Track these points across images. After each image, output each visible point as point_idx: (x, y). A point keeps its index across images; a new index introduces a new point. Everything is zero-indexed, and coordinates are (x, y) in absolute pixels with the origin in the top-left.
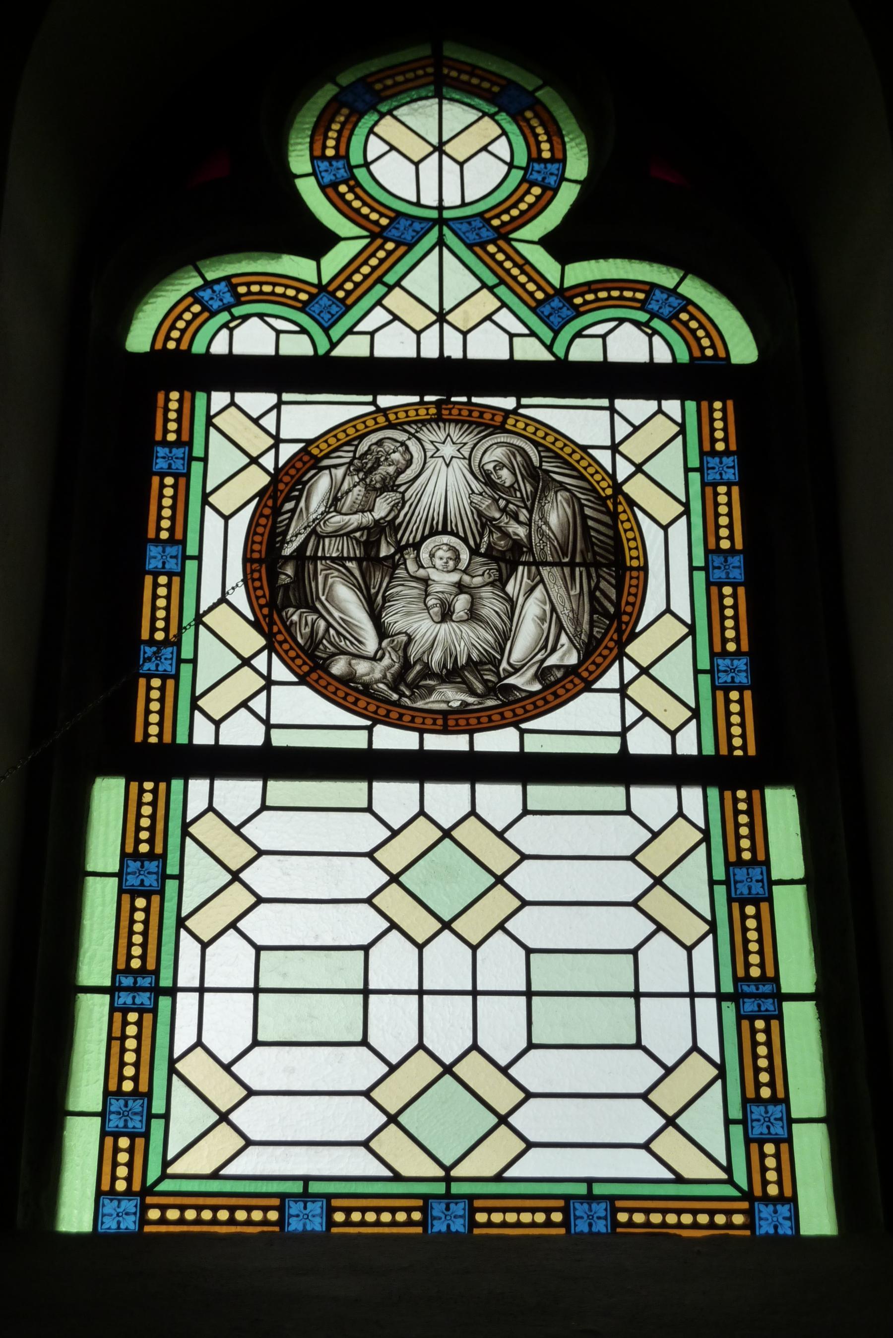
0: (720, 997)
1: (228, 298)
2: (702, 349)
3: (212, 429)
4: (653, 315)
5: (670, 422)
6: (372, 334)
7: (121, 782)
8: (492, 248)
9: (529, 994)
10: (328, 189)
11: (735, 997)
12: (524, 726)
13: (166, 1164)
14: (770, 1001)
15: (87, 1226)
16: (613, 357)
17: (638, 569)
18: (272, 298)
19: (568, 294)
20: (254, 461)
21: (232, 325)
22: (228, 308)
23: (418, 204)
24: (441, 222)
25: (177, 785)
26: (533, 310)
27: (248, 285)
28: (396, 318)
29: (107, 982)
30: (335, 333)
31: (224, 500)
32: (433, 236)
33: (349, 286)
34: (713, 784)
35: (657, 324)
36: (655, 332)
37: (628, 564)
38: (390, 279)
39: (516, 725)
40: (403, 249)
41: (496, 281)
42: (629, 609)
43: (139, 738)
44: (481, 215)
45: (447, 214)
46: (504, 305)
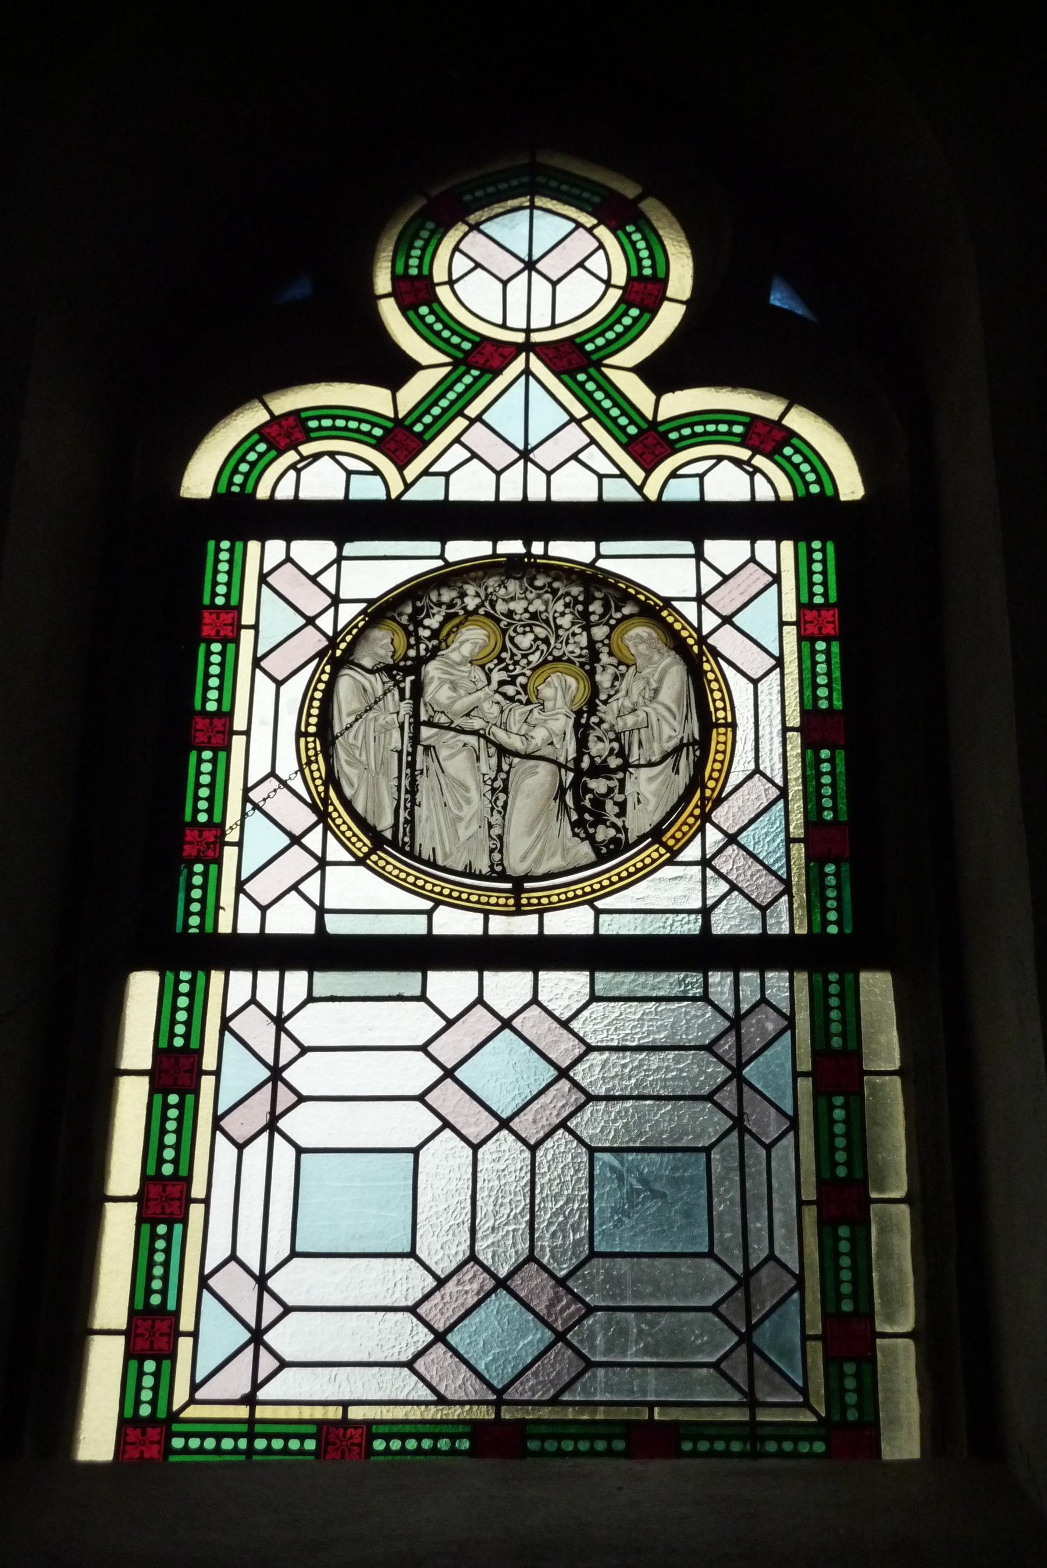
2: (807, 484)
6: (447, 475)
13: (195, 1387)
16: (710, 496)
19: (662, 429)
21: (299, 466)
24: (528, 347)
25: (217, 977)
28: (474, 455)
30: (412, 471)
34: (801, 968)
35: (759, 461)
36: (757, 470)
38: (472, 411)
41: (585, 413)
43: (179, 928)
46: (593, 441)
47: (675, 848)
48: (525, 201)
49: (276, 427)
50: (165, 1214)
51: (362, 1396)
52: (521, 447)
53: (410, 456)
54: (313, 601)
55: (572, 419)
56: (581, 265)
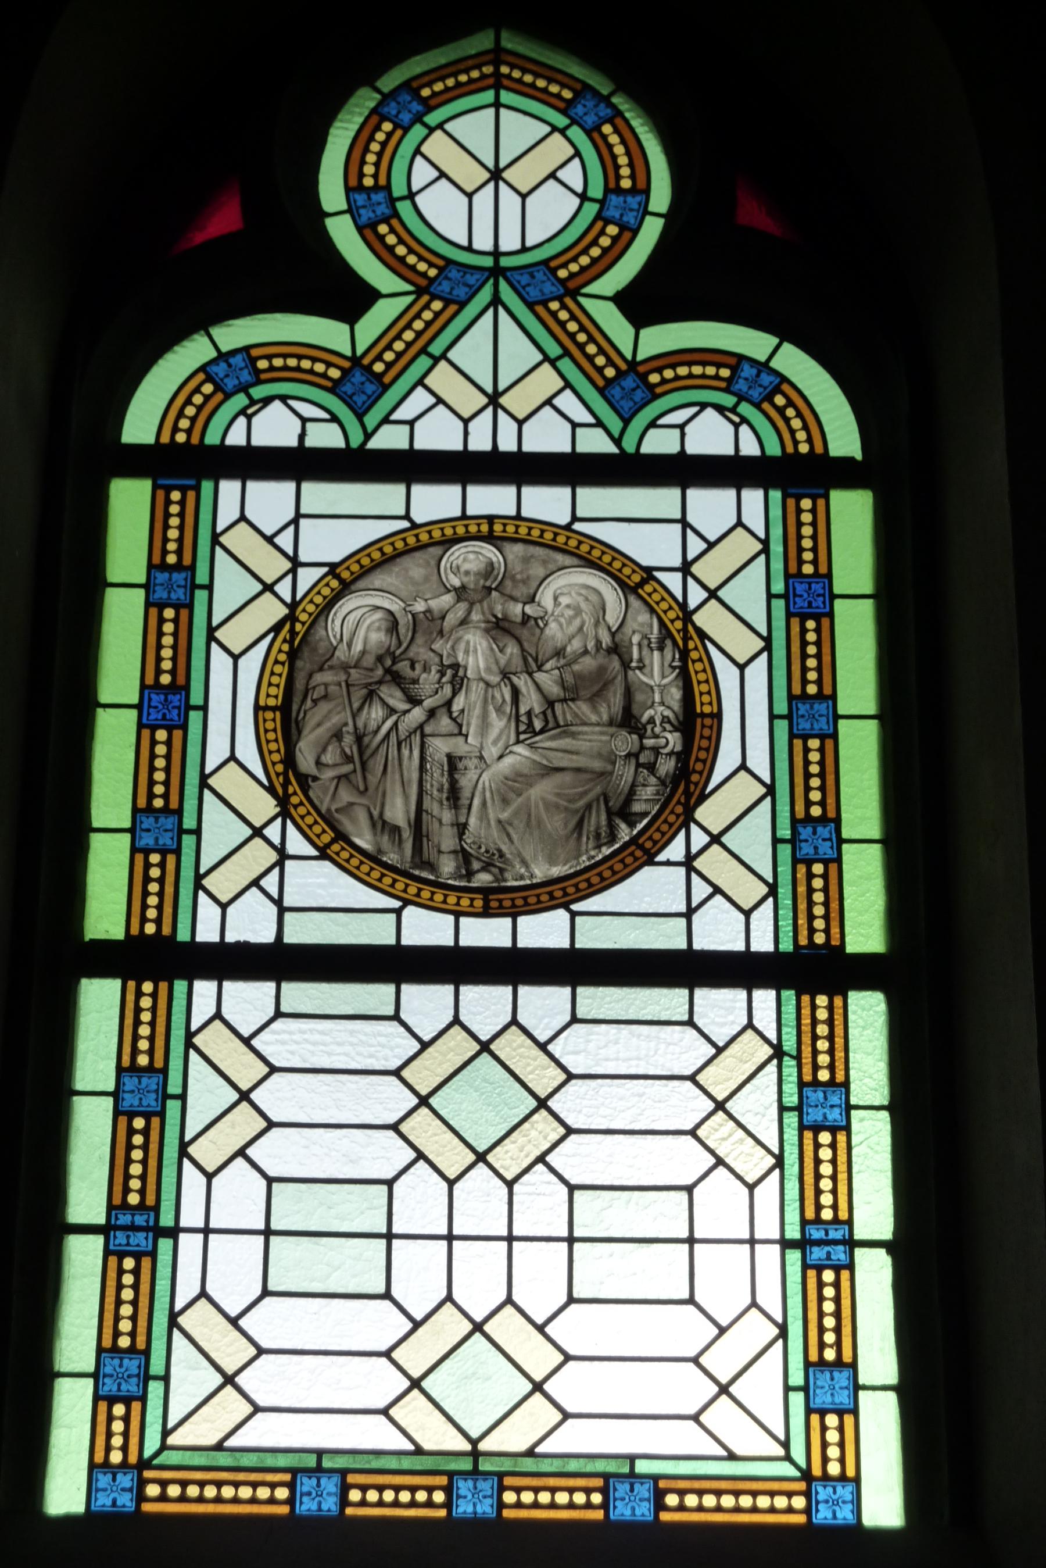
0: (786, 1244)
1: (246, 376)
3: (218, 549)
4: (741, 398)
5: (753, 636)
6: (411, 423)
7: (117, 983)
8: (554, 306)
9: (571, 1240)
10: (366, 230)
11: (803, 1244)
12: (575, 907)
13: (166, 1433)
14: (841, 1248)
15: (78, 1507)
16: (691, 449)
17: (711, 715)
18: (297, 376)
19: (641, 369)
20: (269, 588)
21: (250, 411)
22: (244, 389)
23: (469, 249)
24: (497, 272)
25: (180, 986)
26: (601, 391)
27: (269, 357)
28: (440, 401)
29: (101, 1220)
30: (371, 419)
31: (234, 636)
32: (485, 295)
33: (389, 356)
35: (745, 409)
36: (744, 420)
37: (698, 710)
38: (436, 349)
39: (566, 906)
40: (453, 308)
41: (559, 351)
42: (699, 766)
44: (545, 262)
45: (504, 262)
47: (653, 851)
48: (489, 96)
49: (223, 365)
50: (142, 1106)
51: (271, 1055)
52: (489, 389)
53: (369, 402)
54: (272, 566)
55: (546, 358)
56: (553, 175)
